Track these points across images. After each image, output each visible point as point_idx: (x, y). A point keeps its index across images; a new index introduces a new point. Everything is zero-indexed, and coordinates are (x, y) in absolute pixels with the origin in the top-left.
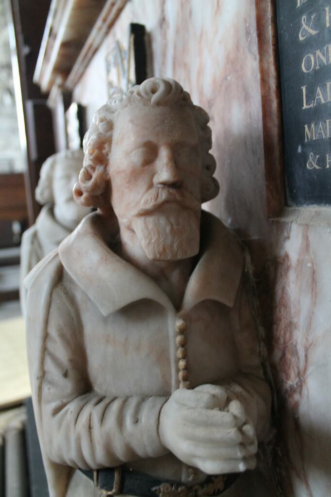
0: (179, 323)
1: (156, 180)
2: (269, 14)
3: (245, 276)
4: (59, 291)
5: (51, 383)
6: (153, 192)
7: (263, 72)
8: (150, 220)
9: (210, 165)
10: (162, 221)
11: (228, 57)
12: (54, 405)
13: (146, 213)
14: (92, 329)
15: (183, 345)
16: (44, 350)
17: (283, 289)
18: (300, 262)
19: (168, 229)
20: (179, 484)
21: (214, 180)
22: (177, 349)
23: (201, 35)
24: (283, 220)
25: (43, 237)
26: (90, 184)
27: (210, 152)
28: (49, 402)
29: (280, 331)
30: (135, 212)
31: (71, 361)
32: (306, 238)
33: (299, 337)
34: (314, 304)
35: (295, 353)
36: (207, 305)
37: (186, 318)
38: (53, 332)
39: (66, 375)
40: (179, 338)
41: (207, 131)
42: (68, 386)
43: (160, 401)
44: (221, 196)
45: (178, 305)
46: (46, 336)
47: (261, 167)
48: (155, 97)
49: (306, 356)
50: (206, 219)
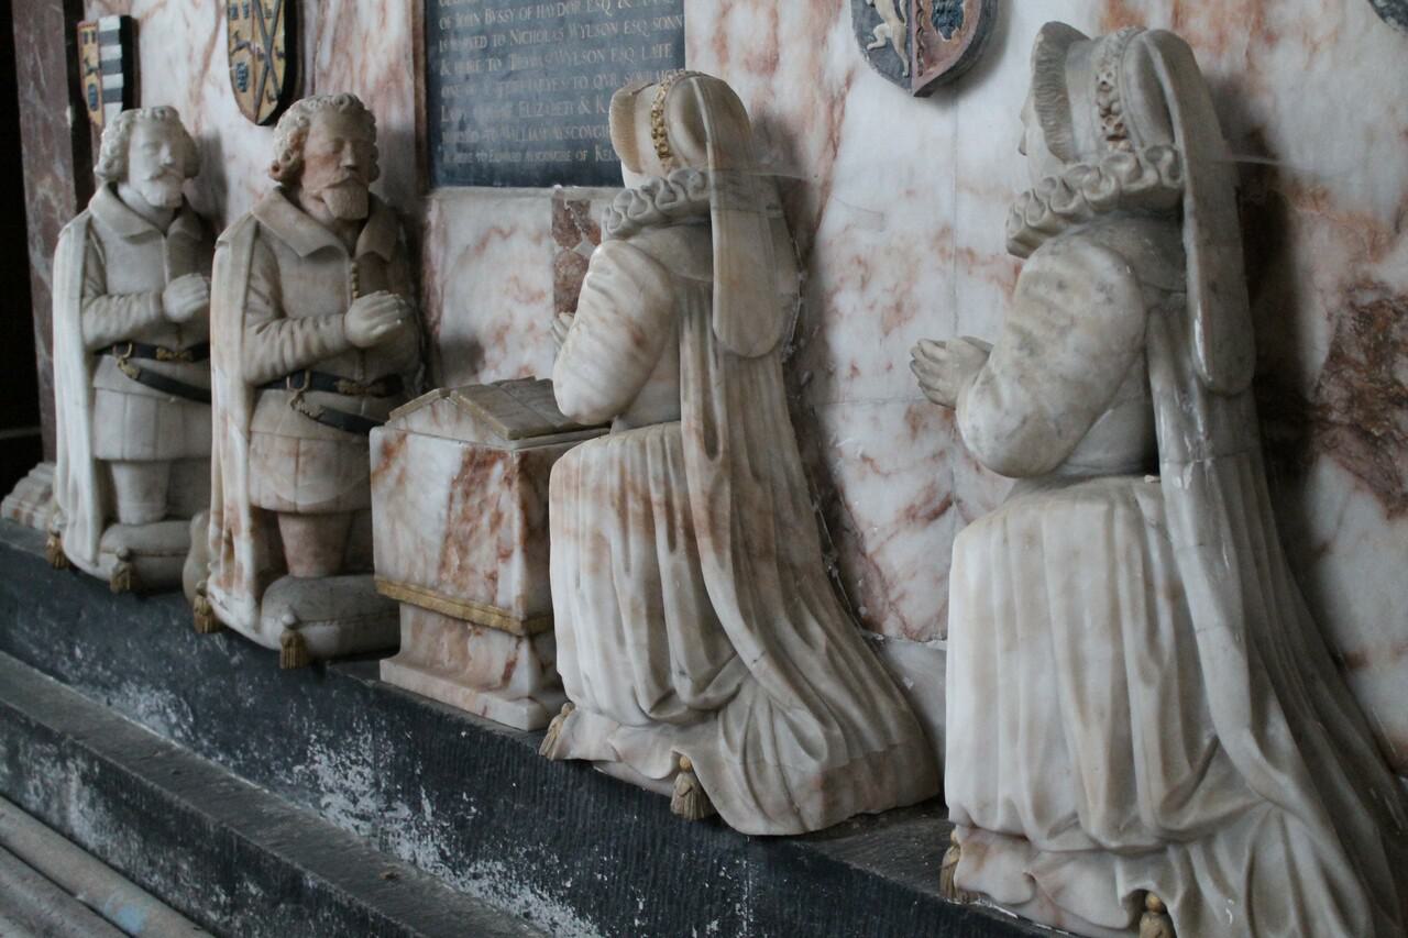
0: (353, 265)
1: (342, 164)
2: (422, 49)
3: (399, 243)
4: (259, 243)
5: (254, 311)
6: (340, 172)
7: (416, 88)
8: (337, 191)
9: (374, 155)
10: (345, 192)
11: (390, 65)
12: (255, 328)
13: (333, 186)
14: (287, 268)
15: (356, 280)
16: (248, 287)
17: (428, 248)
18: (438, 226)
19: (349, 198)
20: (353, 381)
21: (376, 166)
22: (351, 282)
23: (366, 37)
24: (427, 197)
25: (103, 226)
26: (290, 163)
27: (376, 144)
28: (250, 326)
29: (426, 281)
30: (326, 185)
31: (271, 293)
32: (440, 209)
33: (438, 280)
34: (446, 252)
35: (435, 293)
36: (370, 255)
37: (358, 262)
38: (256, 271)
39: (268, 303)
40: (353, 276)
41: (373, 129)
42: (270, 311)
43: (341, 316)
44: (380, 180)
45: (352, 253)
46: (250, 276)
47: (413, 159)
48: (342, 107)
49: (442, 291)
50: (371, 198)
